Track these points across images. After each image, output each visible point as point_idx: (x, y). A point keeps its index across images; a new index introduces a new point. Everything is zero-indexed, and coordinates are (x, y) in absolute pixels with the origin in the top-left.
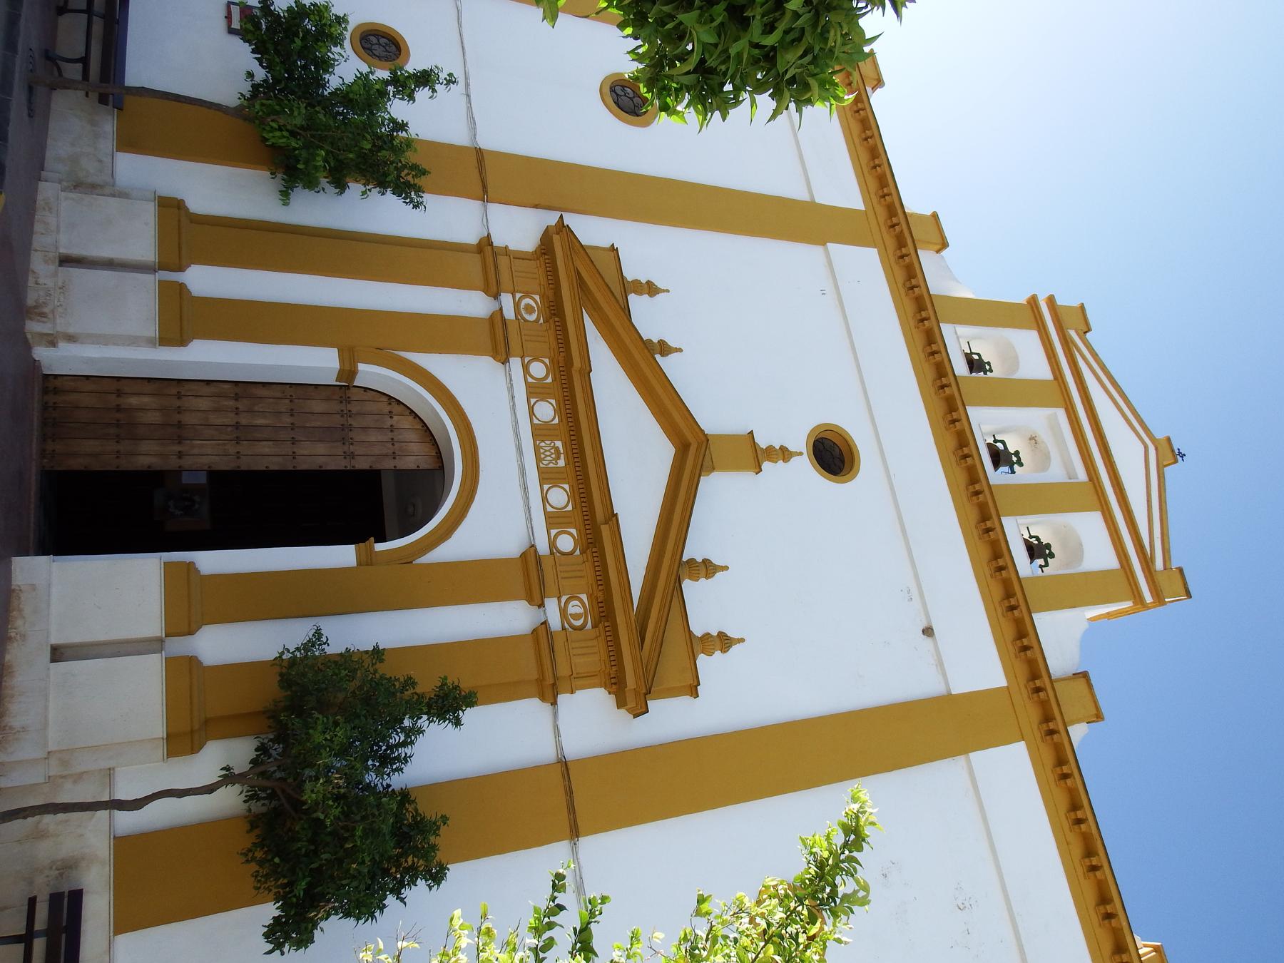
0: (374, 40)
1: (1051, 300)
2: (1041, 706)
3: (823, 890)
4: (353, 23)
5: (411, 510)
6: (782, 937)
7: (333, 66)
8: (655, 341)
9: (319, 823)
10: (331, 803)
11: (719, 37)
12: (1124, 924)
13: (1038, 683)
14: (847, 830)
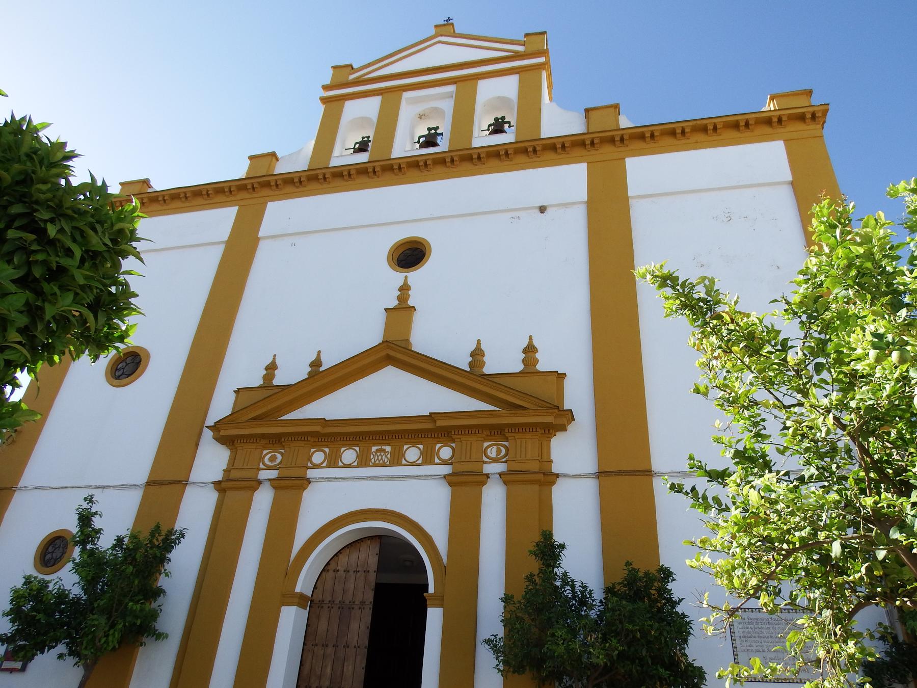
0: (48, 557)
1: (326, 88)
2: (604, 143)
3: (701, 307)
4: (31, 571)
5: (408, 563)
6: (729, 340)
7: (64, 590)
8: (310, 369)
9: (621, 655)
10: (607, 645)
11: (70, 290)
12: (753, 116)
13: (588, 142)
14: (663, 285)
